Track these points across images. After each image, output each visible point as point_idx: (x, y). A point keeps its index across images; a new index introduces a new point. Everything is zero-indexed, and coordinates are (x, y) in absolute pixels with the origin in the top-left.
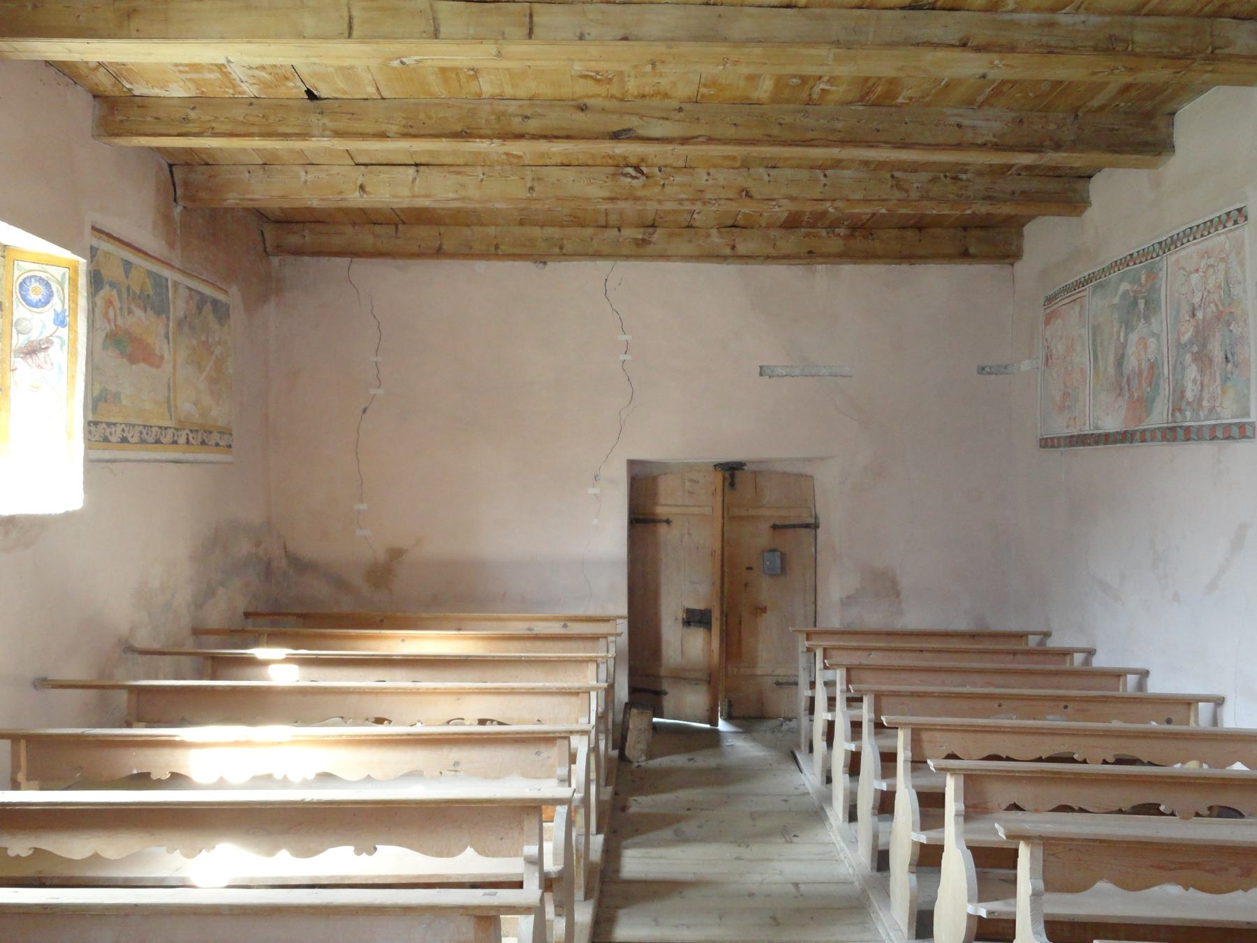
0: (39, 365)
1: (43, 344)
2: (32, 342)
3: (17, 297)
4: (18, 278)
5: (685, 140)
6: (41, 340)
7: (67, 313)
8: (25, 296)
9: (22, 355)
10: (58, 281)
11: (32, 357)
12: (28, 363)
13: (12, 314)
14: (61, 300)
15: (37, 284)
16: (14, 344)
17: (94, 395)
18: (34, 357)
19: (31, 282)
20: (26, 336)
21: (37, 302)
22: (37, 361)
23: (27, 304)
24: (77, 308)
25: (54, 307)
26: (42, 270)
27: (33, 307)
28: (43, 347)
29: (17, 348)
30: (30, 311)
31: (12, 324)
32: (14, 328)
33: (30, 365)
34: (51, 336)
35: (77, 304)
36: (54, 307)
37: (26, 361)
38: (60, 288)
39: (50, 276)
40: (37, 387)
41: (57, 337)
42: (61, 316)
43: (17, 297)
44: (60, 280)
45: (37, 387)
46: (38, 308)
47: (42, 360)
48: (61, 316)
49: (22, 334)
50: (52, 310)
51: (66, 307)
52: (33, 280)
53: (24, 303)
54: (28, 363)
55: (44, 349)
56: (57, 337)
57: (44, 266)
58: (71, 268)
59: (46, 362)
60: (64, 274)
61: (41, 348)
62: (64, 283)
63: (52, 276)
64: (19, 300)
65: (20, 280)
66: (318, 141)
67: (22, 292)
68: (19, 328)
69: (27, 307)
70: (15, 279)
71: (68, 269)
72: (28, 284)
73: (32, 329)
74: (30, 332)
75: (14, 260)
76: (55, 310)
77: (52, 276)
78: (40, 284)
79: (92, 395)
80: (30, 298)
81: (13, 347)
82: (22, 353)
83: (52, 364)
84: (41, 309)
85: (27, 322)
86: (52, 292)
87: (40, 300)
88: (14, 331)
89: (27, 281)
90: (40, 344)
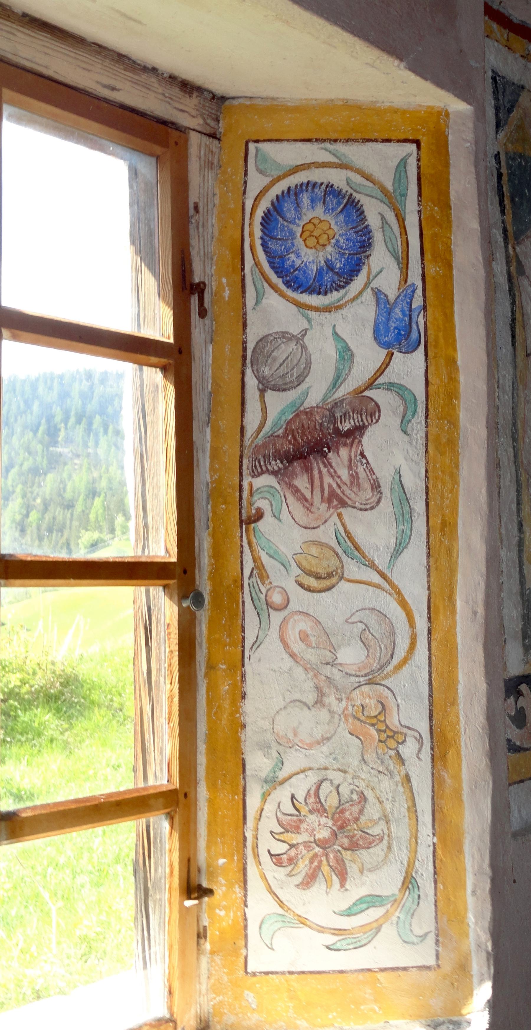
0: (333, 495)
1: (345, 416)
2: (309, 413)
3: (257, 264)
4: (257, 200)
5: (199, 236)
6: (336, 404)
7: (418, 302)
8: (282, 257)
9: (276, 465)
10: (383, 190)
11: (308, 470)
12: (296, 491)
13: (245, 325)
14: (397, 259)
15: (319, 211)
16: (250, 430)
17: (321, 873)
18: (316, 464)
19: (298, 206)
20: (291, 395)
21: (320, 272)
22: (327, 480)
23: (288, 284)
24: (449, 277)
25: (374, 285)
26: (332, 159)
27: (310, 290)
28: (346, 426)
29: (259, 441)
30: (298, 304)
31: (244, 358)
32: (249, 372)
33: (302, 498)
34: (370, 385)
35: (449, 265)
36: (374, 285)
37: (291, 486)
38: (391, 217)
39: (357, 179)
40: (330, 575)
41: (390, 386)
42: (398, 313)
43: (257, 264)
44: (389, 187)
45: (330, 575)
46: (326, 294)
47: (344, 474)
48: (398, 313)
49: (276, 389)
50: (368, 295)
51: (415, 278)
52: (305, 199)
53: (279, 282)
54: (296, 491)
55: (350, 433)
56: (390, 386)
57: (341, 148)
58: (424, 141)
59: (355, 478)
60: (403, 162)
61: (337, 431)
62: (404, 195)
63: (368, 177)
64: (263, 273)
65: (265, 205)
66: (138, 941)
67: (272, 245)
68: (266, 371)
69: (289, 292)
70: (249, 204)
71: (414, 147)
72: (290, 214)
73: (309, 364)
74: (300, 380)
75: (247, 143)
76: (378, 294)
77: (368, 177)
78: (327, 211)
79: (322, 872)
80: (298, 263)
81: (247, 442)
82: (278, 456)
83: (376, 487)
84: (335, 296)
85: (292, 346)
86: (367, 231)
87: (330, 266)
88: (251, 382)
89: (289, 208)
90: (333, 419)
